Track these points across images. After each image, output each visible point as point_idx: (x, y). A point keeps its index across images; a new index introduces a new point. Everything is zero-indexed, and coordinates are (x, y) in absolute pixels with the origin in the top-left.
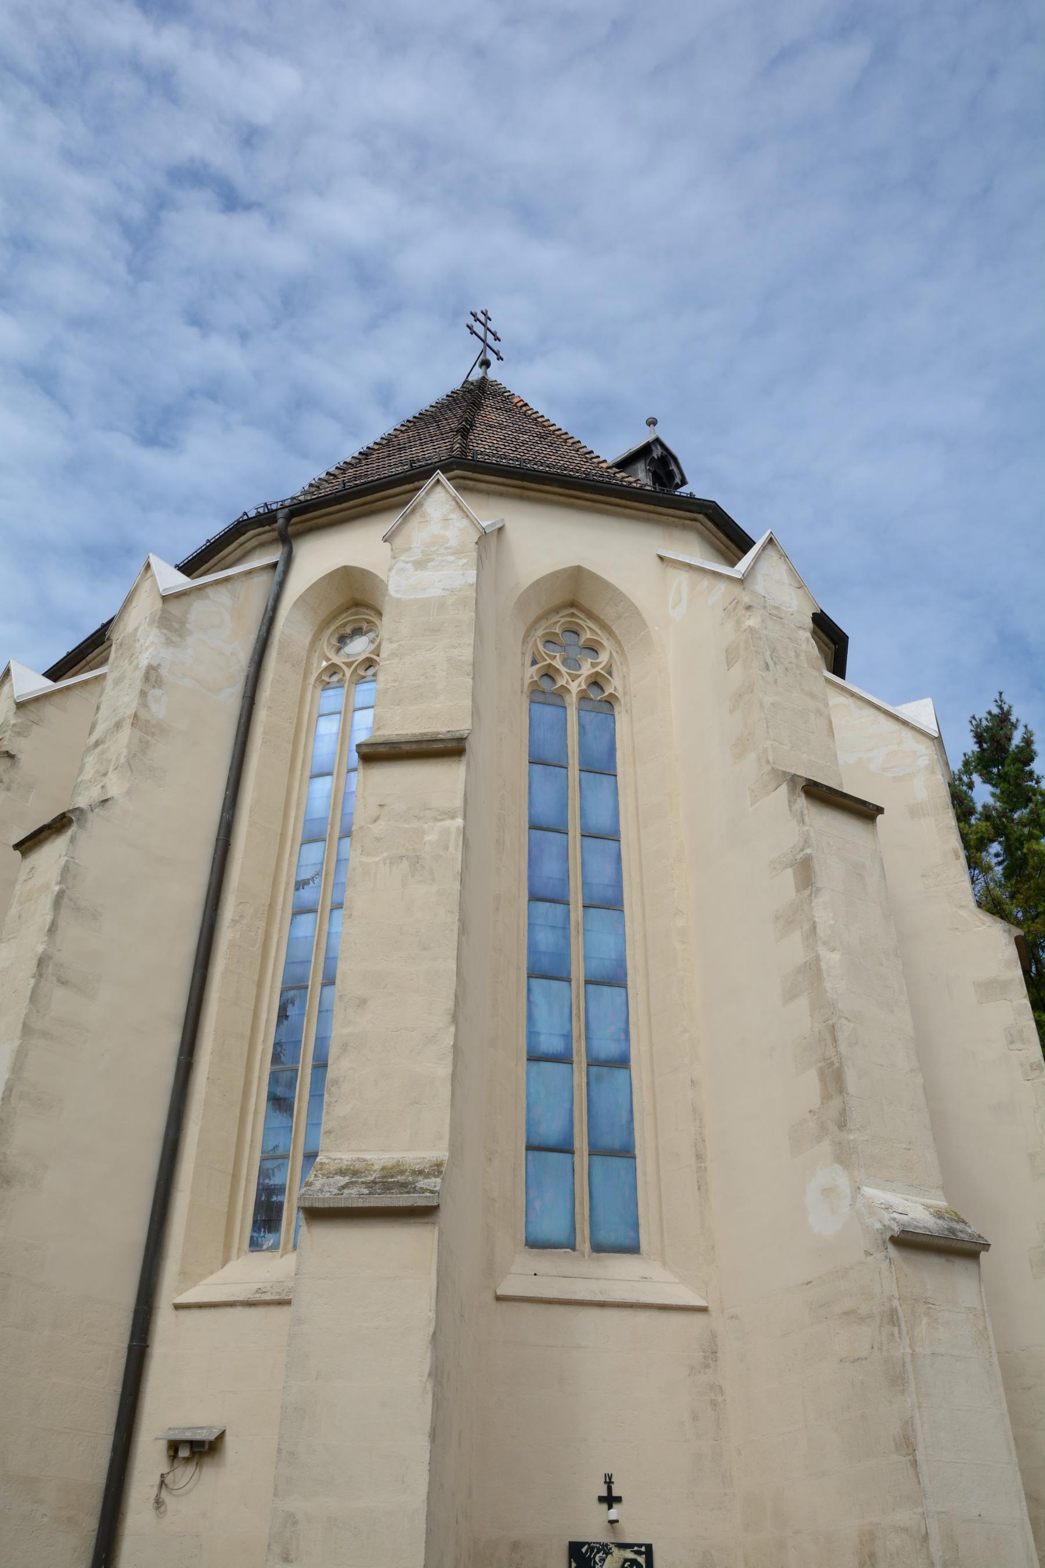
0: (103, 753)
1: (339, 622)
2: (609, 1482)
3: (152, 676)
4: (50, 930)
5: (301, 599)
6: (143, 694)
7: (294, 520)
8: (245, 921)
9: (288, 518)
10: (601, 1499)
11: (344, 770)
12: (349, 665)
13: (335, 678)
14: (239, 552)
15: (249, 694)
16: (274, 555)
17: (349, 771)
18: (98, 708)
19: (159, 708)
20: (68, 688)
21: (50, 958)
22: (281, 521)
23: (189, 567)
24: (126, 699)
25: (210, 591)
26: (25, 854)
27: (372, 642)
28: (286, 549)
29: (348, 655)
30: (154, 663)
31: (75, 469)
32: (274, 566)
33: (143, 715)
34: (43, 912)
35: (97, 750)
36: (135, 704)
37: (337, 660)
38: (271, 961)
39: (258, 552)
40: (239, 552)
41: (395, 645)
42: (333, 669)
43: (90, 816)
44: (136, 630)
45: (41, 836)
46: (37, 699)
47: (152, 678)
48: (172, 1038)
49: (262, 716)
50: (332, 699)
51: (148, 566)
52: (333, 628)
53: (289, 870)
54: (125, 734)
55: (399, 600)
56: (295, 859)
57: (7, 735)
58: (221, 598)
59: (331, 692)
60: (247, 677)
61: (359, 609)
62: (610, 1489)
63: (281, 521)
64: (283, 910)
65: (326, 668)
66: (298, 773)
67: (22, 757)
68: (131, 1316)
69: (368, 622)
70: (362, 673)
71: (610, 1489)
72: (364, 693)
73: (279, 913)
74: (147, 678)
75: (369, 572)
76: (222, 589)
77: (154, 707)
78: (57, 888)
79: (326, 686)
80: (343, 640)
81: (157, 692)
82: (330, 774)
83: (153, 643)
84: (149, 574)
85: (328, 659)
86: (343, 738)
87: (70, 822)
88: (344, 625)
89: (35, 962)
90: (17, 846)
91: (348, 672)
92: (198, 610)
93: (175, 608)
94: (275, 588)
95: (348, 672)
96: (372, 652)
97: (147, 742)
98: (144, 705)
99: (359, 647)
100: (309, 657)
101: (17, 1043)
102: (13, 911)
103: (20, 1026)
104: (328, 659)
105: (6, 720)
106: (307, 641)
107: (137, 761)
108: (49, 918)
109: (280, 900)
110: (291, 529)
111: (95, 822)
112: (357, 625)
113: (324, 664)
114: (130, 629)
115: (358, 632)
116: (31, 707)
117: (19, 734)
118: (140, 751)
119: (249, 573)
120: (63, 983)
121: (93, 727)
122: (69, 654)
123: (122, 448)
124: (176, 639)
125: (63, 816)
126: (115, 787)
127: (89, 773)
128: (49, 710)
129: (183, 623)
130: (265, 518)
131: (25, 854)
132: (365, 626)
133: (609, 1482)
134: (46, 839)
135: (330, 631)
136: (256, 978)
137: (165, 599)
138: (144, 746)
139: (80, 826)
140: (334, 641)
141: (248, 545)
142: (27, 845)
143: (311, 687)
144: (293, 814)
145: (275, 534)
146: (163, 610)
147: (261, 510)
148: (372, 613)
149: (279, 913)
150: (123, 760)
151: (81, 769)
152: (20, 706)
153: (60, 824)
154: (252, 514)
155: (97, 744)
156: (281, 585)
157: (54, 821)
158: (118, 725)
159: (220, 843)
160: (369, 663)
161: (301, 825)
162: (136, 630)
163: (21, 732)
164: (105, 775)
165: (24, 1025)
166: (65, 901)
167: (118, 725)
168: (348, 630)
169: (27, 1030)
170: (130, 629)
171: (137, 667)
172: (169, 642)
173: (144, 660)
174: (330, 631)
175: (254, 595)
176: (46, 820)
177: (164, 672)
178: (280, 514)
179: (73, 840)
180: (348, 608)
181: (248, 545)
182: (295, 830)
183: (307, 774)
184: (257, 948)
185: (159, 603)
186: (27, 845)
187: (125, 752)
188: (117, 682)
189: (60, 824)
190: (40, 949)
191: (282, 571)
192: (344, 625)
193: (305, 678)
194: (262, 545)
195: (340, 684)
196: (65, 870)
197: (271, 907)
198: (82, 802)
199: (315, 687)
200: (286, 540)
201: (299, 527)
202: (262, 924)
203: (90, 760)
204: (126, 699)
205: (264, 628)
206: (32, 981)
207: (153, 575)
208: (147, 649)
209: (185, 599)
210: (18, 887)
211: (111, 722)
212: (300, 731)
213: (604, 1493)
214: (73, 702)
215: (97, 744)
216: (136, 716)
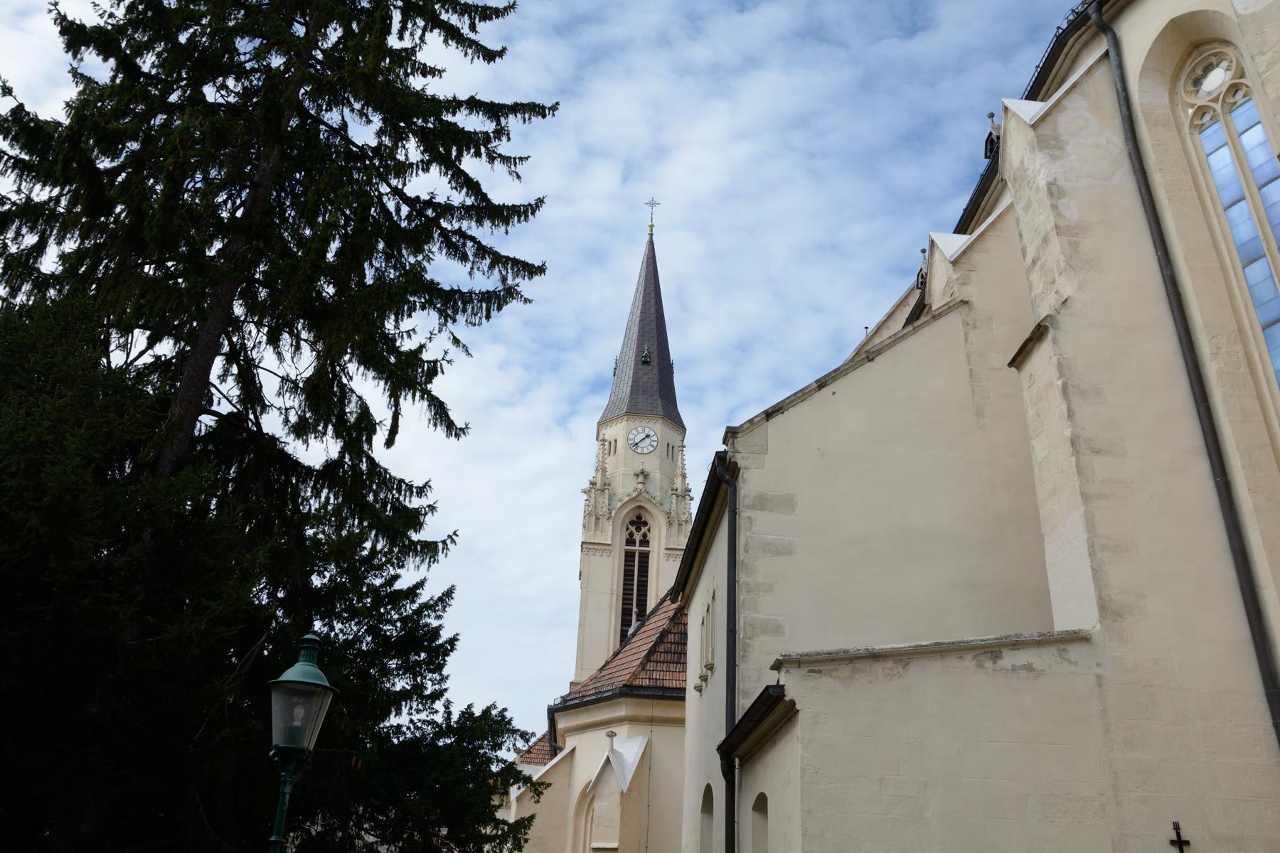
0: (1042, 267)
1: (1187, 70)
2: (1177, 827)
3: (1054, 190)
4: (1069, 416)
5: (1145, 69)
6: (1054, 207)
7: (1104, 9)
8: (1223, 351)
9: (1099, 10)
10: (1172, 842)
11: (1255, 189)
12: (1215, 100)
13: (1207, 118)
14: (1068, 61)
15: (1138, 167)
16: (1102, 46)
17: (1260, 189)
18: (1021, 236)
19: (1072, 213)
20: (982, 234)
21: (1078, 437)
22: (1094, 16)
23: (1033, 93)
24: (1041, 218)
25: (1065, 102)
26: (1019, 368)
27: (1228, 69)
28: (1110, 36)
29: (1209, 93)
30: (1051, 180)
31: (868, 84)
32: (1106, 54)
33: (1062, 223)
34: (1058, 405)
35: (1037, 267)
36: (1052, 218)
37: (1200, 102)
38: (1261, 375)
39: (1084, 52)
40: (1068, 61)
41: (1270, 55)
42: (1201, 111)
43: (1059, 317)
44: (1022, 162)
45: (1027, 349)
46: (964, 253)
47: (1055, 192)
48: (1203, 467)
49: (1158, 181)
50: (1214, 134)
51: (1006, 109)
52: (1183, 78)
53: (1242, 295)
54: (1055, 244)
55: (1253, 15)
56: (1244, 284)
57: (955, 288)
58: (1077, 103)
59: (1209, 131)
60: (1130, 155)
61: (1201, 49)
62: (1178, 834)
63: (1094, 16)
64: (1252, 329)
65: (1195, 114)
66: (1212, 211)
67: (972, 299)
68: (1265, 699)
69: (1215, 55)
70: (1232, 100)
71: (1178, 834)
72: (1241, 117)
73: (1250, 333)
74: (1051, 194)
75: (1192, 15)
76: (1073, 96)
77: (1067, 214)
78: (1060, 382)
79: (1202, 128)
80: (1197, 83)
81: (1064, 200)
82: (1243, 199)
83: (1042, 165)
84: (1010, 115)
85: (1192, 106)
86: (1241, 164)
87: (1046, 328)
88: (1194, 69)
89: (1068, 444)
90: (1011, 364)
91: (1218, 107)
92: (1063, 121)
93: (1045, 129)
94: (1117, 72)
95: (1218, 107)
96: (1233, 78)
97: (1075, 243)
98: (1059, 215)
99: (1217, 79)
100: (1174, 113)
101: (1082, 509)
102: (1031, 413)
103: (1079, 497)
104: (1192, 106)
105: (949, 278)
106: (1166, 100)
107: (1075, 260)
108: (1064, 407)
109: (1246, 322)
110: (1105, 17)
111: (1065, 320)
112: (1205, 64)
113: (1191, 111)
114: (1016, 164)
115: (1208, 69)
116: (963, 261)
117: (964, 284)
118: (1073, 249)
119: (1089, 71)
120: (1097, 452)
121: (1024, 252)
122: (965, 210)
123: (895, 49)
124: (1058, 153)
125: (1039, 326)
126: (1067, 287)
127: (1038, 287)
128: (977, 257)
129: (1057, 138)
130: (1078, 21)
131: (1019, 368)
132: (1214, 60)
133: (1177, 827)
134: (1032, 349)
135: (1182, 81)
136: (1254, 393)
137: (1034, 126)
138: (1074, 247)
139: (1055, 329)
140: (1191, 88)
141: (1074, 52)
142: (1019, 360)
143: (1188, 137)
144: (1223, 247)
145: (1094, 28)
146: (1037, 136)
147: (1071, 17)
148: (1216, 45)
149: (1250, 333)
150: (1063, 264)
151: (1030, 286)
152: (955, 263)
153: (1039, 333)
154: (1064, 26)
155: (1034, 262)
156: (1121, 66)
157: (1034, 332)
158: (1045, 240)
159: (1172, 297)
160: (1234, 89)
161: (1235, 253)
162: (1022, 162)
163: (964, 282)
164: (1053, 282)
165: (1082, 494)
166: (1071, 390)
167: (1045, 240)
168: (1199, 71)
169: (1085, 497)
170: (1016, 164)
171: (1038, 189)
172: (1054, 158)
173: (1042, 181)
174: (1182, 81)
175: (1103, 85)
176: (1027, 335)
177: (1061, 183)
178: (1090, 11)
179: (1055, 341)
180: (1190, 54)
181: (1074, 52)
182: (1232, 259)
183: (1220, 209)
184: (1244, 368)
185: (1031, 133)
186: (1019, 360)
187: (1062, 258)
188: (1027, 208)
189: (1039, 333)
190: (1068, 432)
191: (1115, 57)
192: (1194, 69)
193: (1179, 131)
194: (1086, 45)
195: (1214, 119)
196: (1060, 366)
197: (1241, 330)
198: (1043, 312)
199: (1191, 134)
200: (1106, 28)
201: (1112, 12)
202: (1239, 347)
203: (1035, 277)
204: (1041, 218)
205: (1124, 109)
206: (1073, 459)
207: (1014, 114)
208: (1039, 172)
209: (1049, 118)
210: (1025, 394)
211: (1038, 241)
212: (1197, 174)
213: (1174, 837)
214: (991, 242)
215: (1034, 262)
216: (1057, 226)
